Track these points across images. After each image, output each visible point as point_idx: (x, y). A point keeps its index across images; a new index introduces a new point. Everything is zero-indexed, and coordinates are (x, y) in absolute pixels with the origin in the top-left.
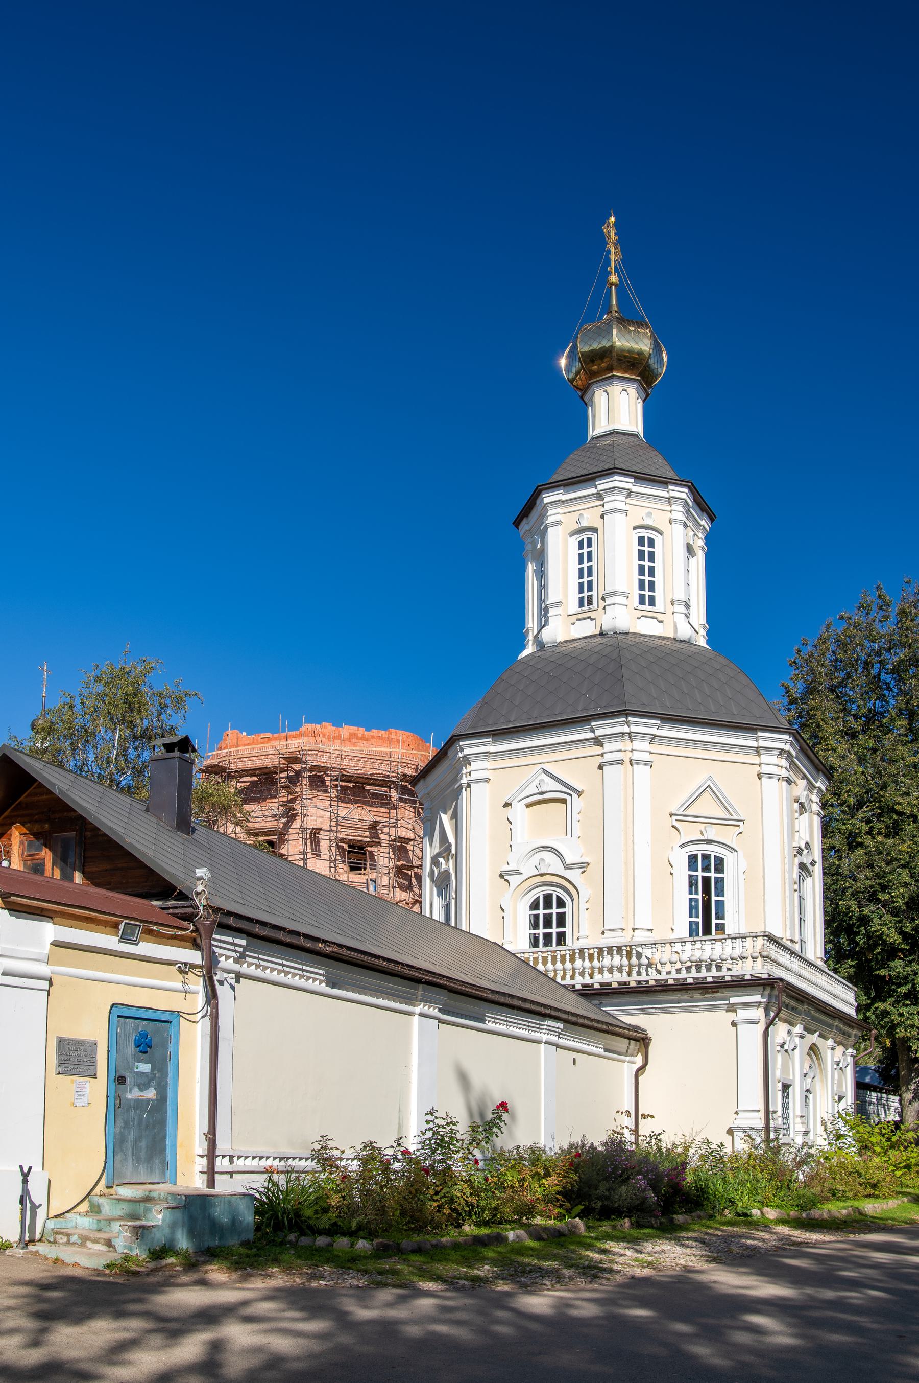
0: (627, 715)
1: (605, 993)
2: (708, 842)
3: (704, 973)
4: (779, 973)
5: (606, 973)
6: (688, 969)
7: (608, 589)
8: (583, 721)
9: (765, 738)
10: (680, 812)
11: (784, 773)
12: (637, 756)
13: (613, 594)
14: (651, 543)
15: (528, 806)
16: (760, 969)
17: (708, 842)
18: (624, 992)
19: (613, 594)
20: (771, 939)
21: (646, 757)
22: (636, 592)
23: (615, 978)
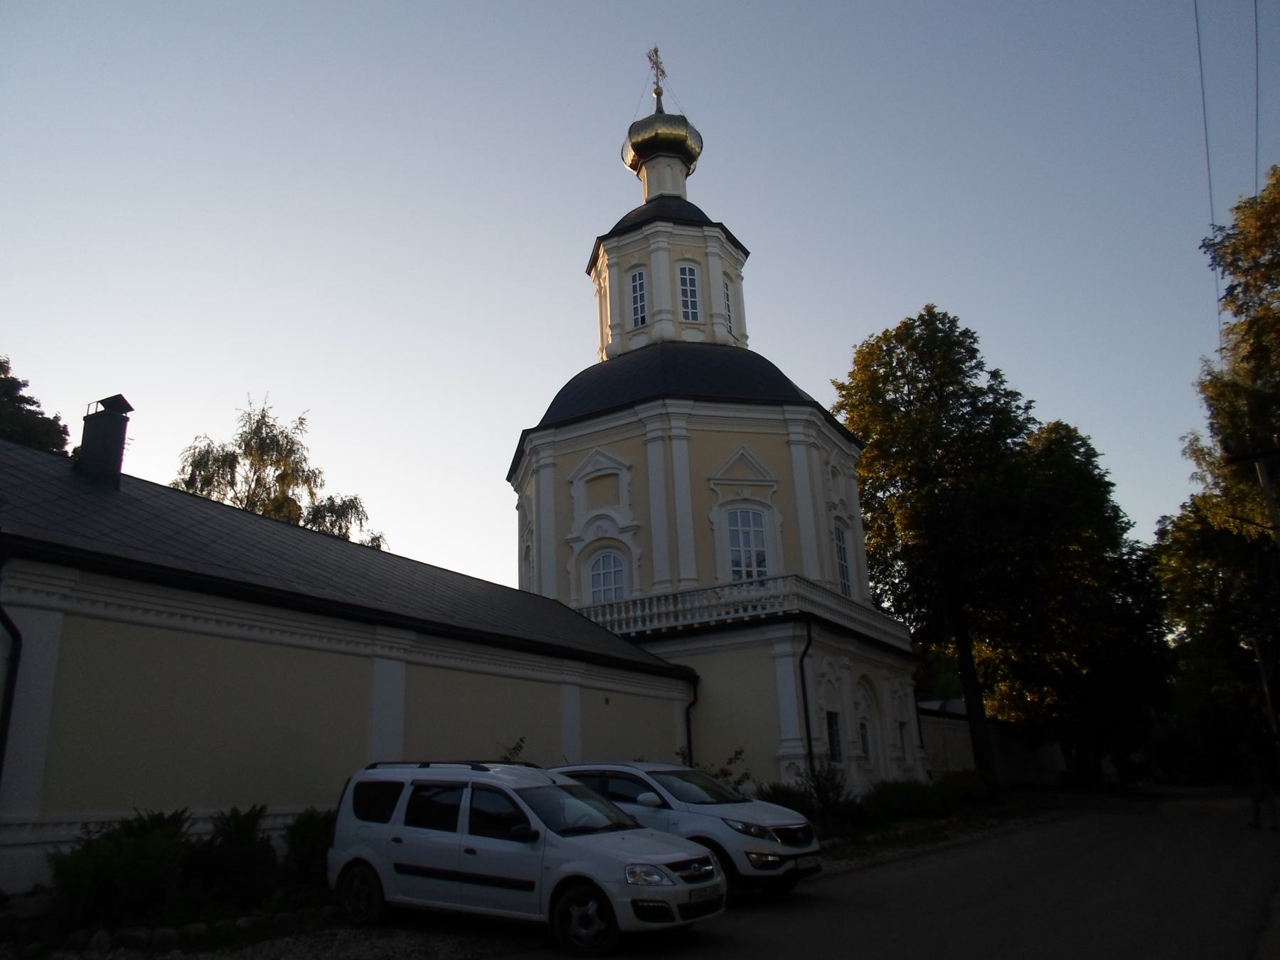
0: (663, 398)
1: (642, 638)
2: (745, 500)
3: (741, 614)
4: (807, 608)
5: (656, 621)
6: (745, 610)
7: (656, 309)
8: (629, 405)
9: (790, 412)
10: (718, 476)
11: (811, 440)
12: (674, 432)
13: (660, 312)
14: (692, 272)
15: (588, 482)
16: (794, 606)
17: (745, 500)
18: (673, 634)
19: (660, 312)
20: (800, 579)
21: (684, 432)
22: (681, 310)
23: (664, 624)
